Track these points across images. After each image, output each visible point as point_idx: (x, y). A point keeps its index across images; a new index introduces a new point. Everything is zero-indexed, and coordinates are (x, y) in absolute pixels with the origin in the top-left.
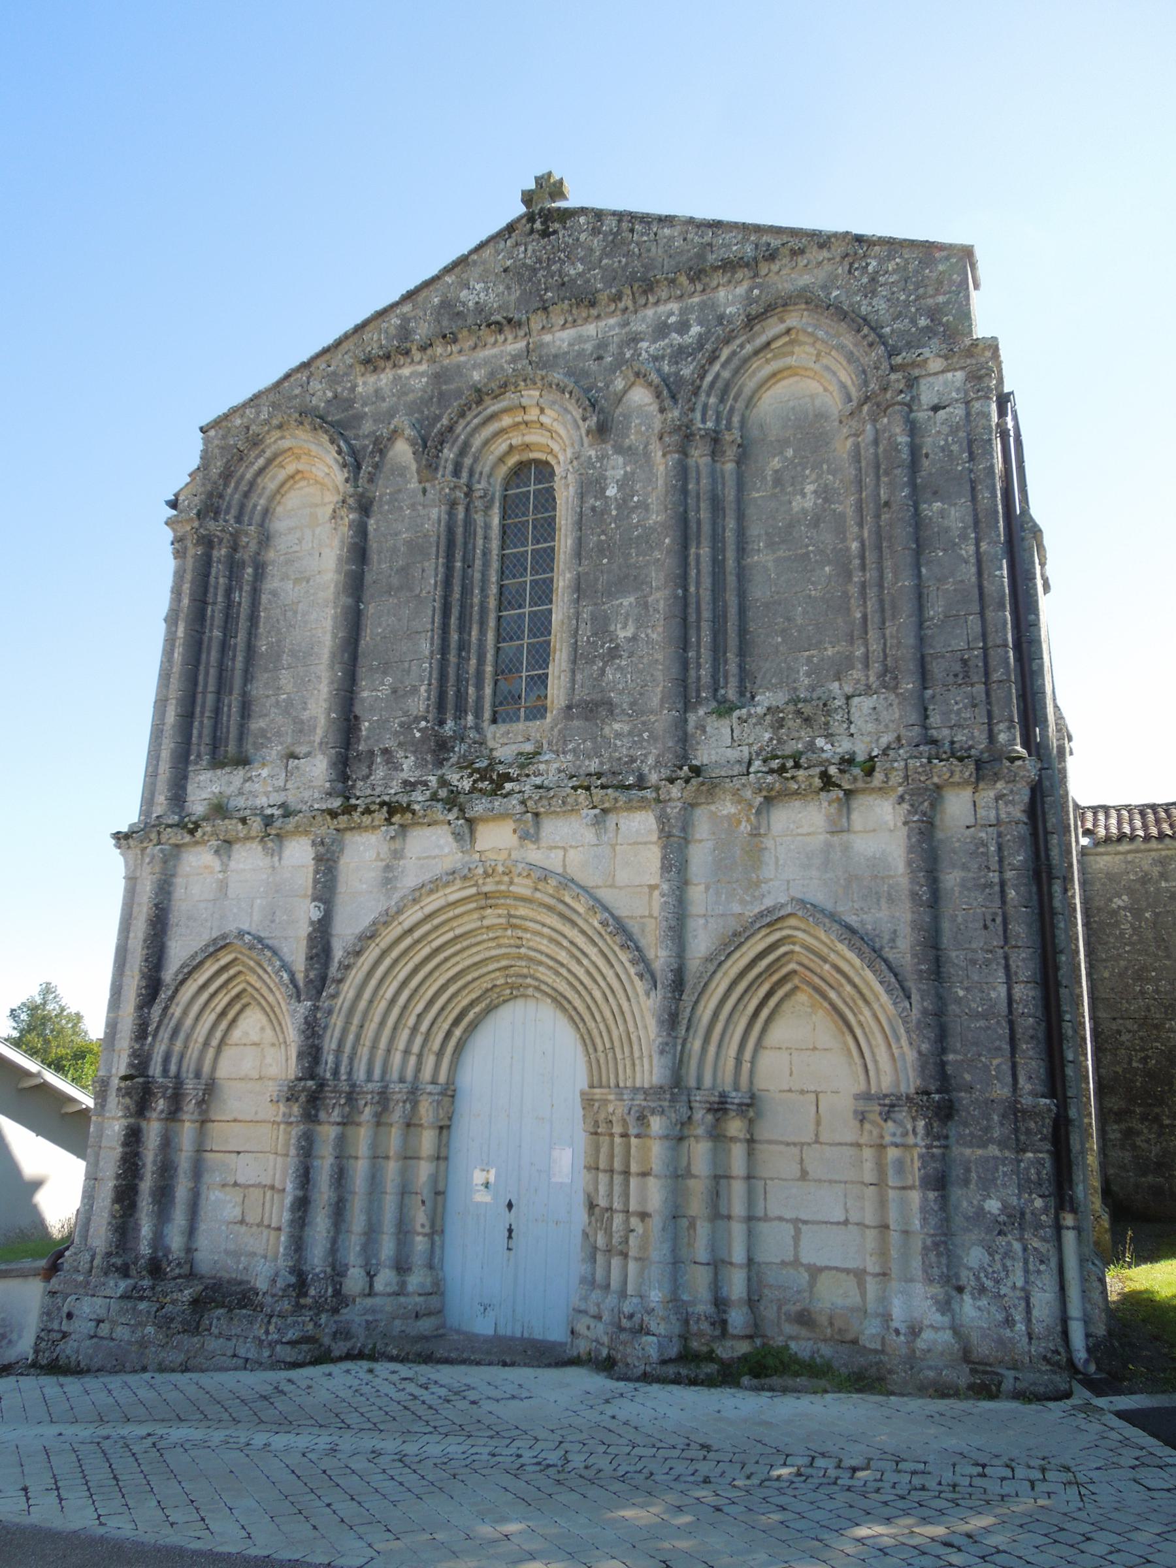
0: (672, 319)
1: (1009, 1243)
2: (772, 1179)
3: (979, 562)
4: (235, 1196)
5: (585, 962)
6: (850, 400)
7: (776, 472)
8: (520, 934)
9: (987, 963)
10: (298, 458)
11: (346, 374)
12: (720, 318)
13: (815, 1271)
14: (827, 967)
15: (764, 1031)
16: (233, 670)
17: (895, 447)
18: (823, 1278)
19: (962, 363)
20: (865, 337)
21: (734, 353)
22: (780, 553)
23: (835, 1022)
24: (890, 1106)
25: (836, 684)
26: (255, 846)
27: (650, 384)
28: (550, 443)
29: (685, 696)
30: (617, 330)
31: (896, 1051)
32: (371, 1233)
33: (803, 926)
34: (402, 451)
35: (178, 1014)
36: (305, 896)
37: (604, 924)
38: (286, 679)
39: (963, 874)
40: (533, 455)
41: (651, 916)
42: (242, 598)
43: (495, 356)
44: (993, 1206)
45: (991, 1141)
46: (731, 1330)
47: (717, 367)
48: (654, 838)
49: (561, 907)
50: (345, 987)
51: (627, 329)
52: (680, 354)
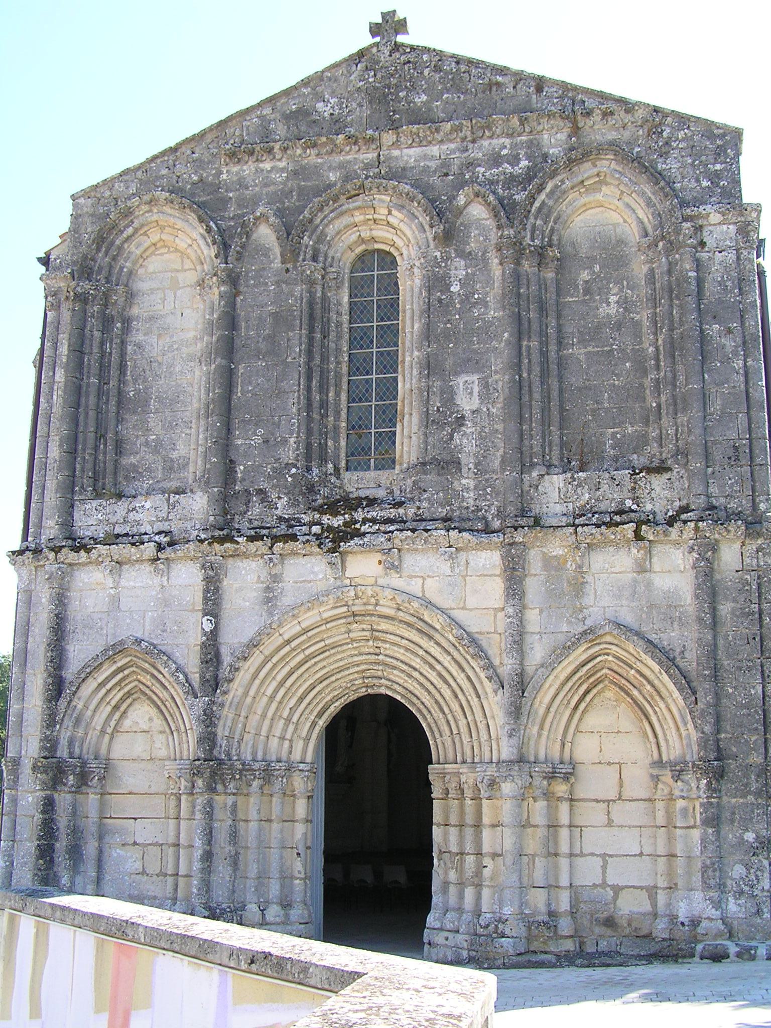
0: (504, 152)
1: (760, 861)
2: (586, 827)
3: (746, 374)
4: (136, 853)
5: (438, 667)
6: (646, 235)
7: (586, 282)
8: (380, 644)
9: (749, 669)
10: (162, 228)
11: (209, 162)
12: (545, 156)
13: (617, 890)
14: (633, 672)
15: (581, 719)
16: (107, 411)
17: (687, 279)
18: (623, 894)
19: (734, 220)
20: (662, 189)
21: (556, 186)
22: (590, 349)
23: (634, 712)
24: (678, 770)
25: (635, 456)
26: (147, 568)
27: (489, 205)
28: (395, 238)
29: (522, 461)
30: (457, 155)
31: (684, 733)
32: (263, 876)
33: (616, 642)
34: (266, 234)
35: (80, 706)
36: (193, 610)
37: (460, 639)
38: (153, 421)
39: (733, 605)
40: (377, 246)
41: (495, 632)
42: (112, 348)
43: (349, 162)
44: (750, 836)
45: (750, 792)
46: (560, 933)
47: (543, 196)
48: (498, 572)
49: (420, 625)
50: (235, 685)
51: (466, 154)
52: (511, 181)
